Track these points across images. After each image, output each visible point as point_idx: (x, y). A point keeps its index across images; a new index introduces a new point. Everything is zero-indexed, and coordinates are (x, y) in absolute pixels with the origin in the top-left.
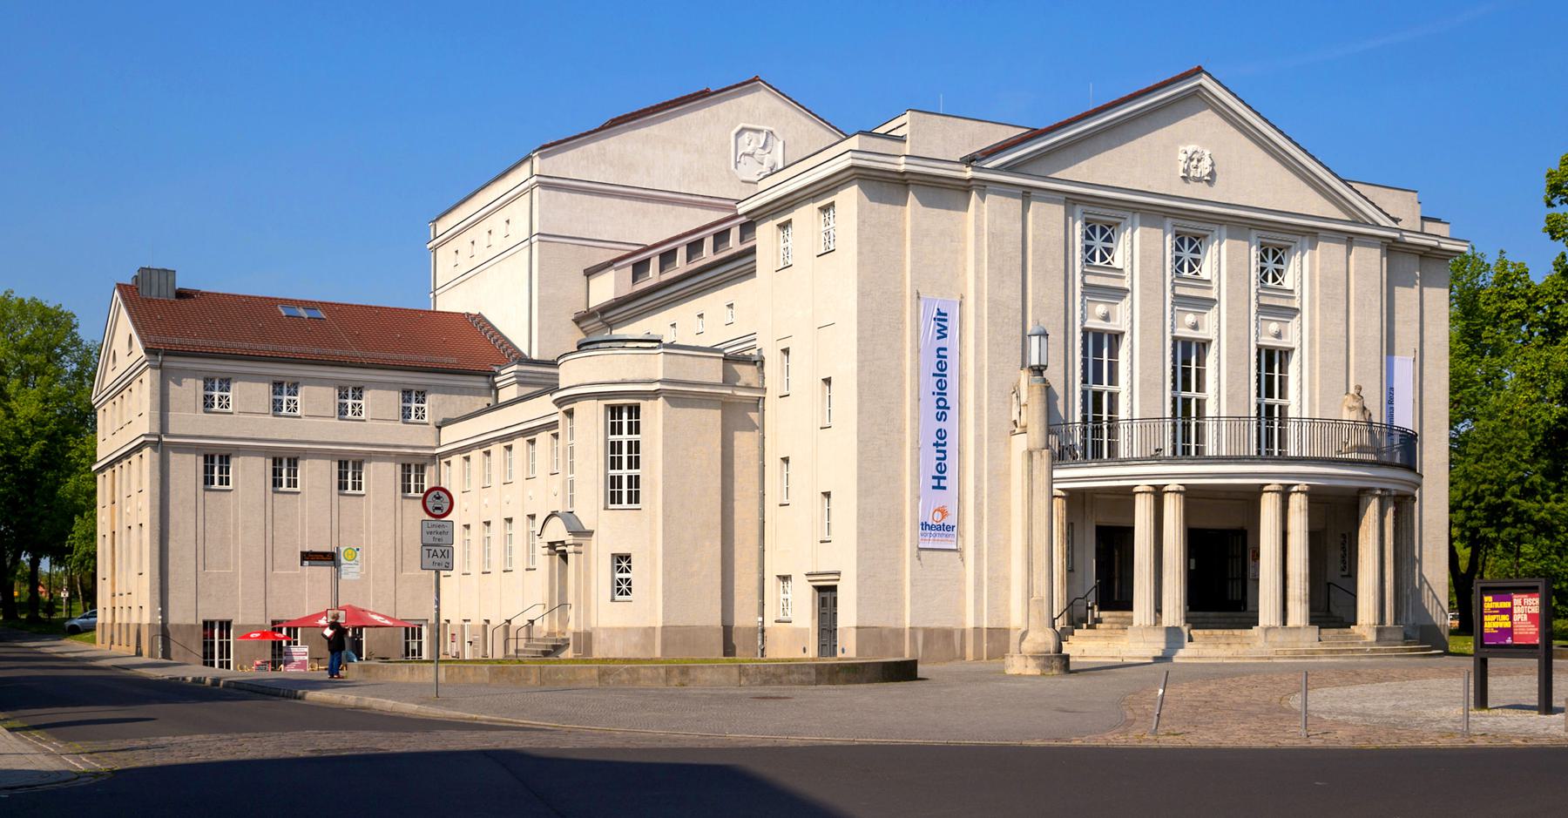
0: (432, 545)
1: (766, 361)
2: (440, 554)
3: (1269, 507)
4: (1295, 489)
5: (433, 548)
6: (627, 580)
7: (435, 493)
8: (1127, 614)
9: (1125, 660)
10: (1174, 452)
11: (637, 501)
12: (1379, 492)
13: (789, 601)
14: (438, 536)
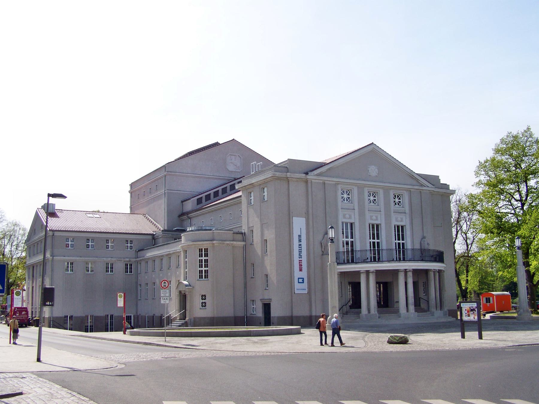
0: (164, 297)
2: (166, 299)
4: (408, 270)
5: (164, 297)
6: (205, 302)
7: (164, 281)
8: (359, 310)
9: (428, 349)
10: (397, 259)
11: (207, 278)
12: (433, 270)
13: (255, 308)
14: (165, 294)
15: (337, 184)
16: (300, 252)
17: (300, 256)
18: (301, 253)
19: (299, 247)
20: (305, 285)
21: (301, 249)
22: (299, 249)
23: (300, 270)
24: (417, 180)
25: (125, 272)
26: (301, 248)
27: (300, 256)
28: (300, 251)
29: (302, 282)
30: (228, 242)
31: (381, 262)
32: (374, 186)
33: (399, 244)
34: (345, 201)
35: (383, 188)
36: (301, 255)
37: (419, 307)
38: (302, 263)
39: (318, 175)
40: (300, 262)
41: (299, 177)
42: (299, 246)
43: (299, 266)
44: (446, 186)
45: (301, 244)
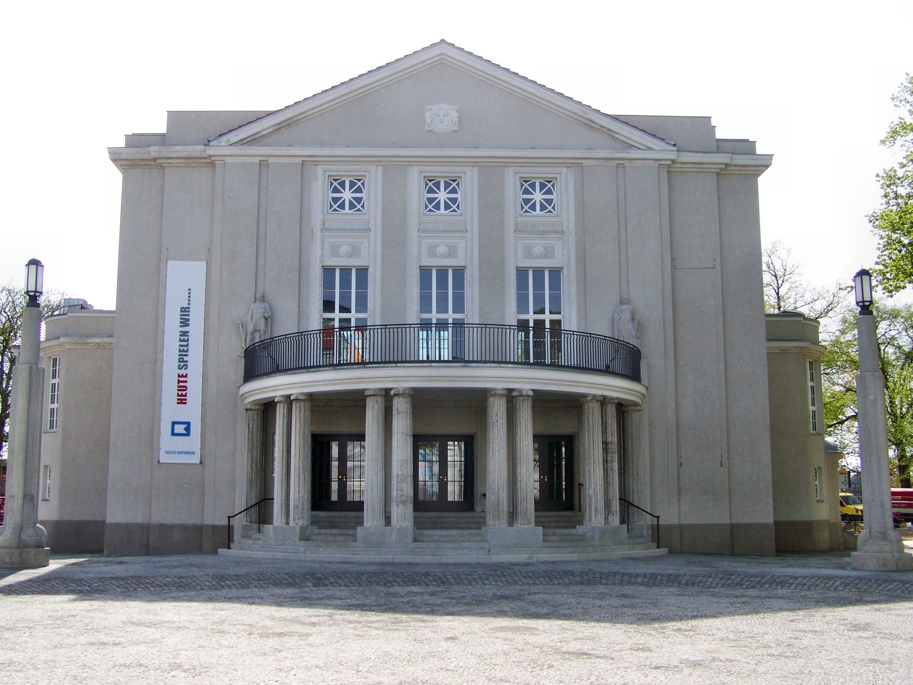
4: (392, 393)
8: (359, 514)
15: (305, 165)
16: (183, 352)
17: (183, 363)
18: (187, 355)
19: (181, 340)
20: (194, 442)
21: (185, 343)
22: (180, 346)
23: (178, 399)
24: (610, 133)
26: (187, 341)
27: (183, 363)
28: (183, 351)
29: (185, 432)
30: (97, 340)
31: (313, 369)
32: (463, 160)
34: (535, 210)
35: (473, 162)
36: (187, 362)
38: (186, 382)
39: (243, 142)
40: (181, 379)
41: (187, 153)
42: (182, 338)
43: (178, 390)
44: (746, 147)
45: (188, 332)
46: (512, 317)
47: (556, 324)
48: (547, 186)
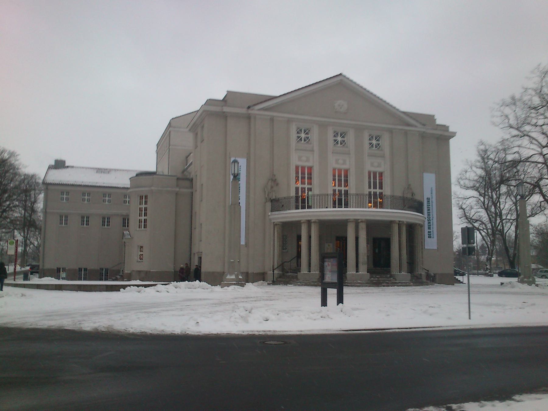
1: (193, 179)
3: (396, 228)
15: (289, 121)
25: (59, 224)
33: (340, 191)
37: (42, 276)
39: (259, 110)
44: (445, 128)
46: (367, 191)
47: (346, 192)
48: (307, 132)
